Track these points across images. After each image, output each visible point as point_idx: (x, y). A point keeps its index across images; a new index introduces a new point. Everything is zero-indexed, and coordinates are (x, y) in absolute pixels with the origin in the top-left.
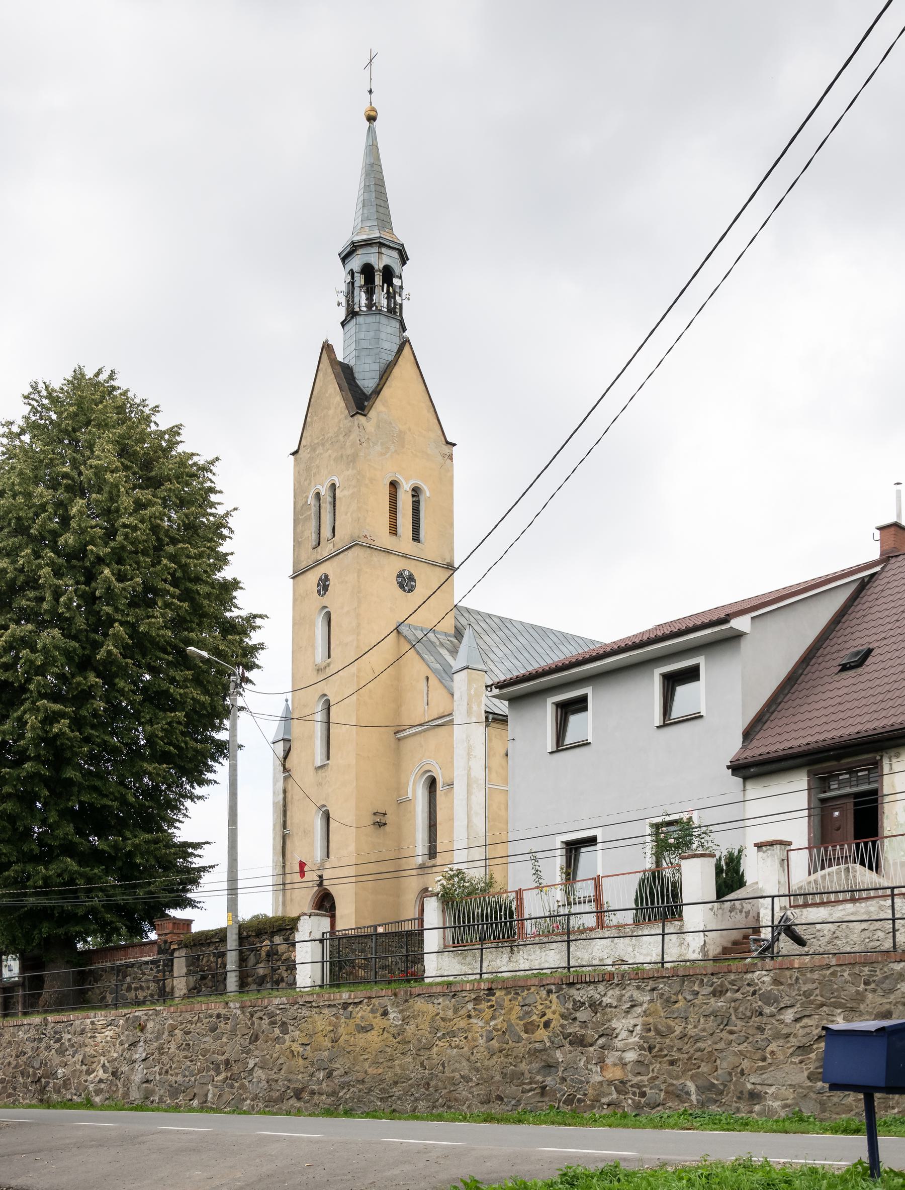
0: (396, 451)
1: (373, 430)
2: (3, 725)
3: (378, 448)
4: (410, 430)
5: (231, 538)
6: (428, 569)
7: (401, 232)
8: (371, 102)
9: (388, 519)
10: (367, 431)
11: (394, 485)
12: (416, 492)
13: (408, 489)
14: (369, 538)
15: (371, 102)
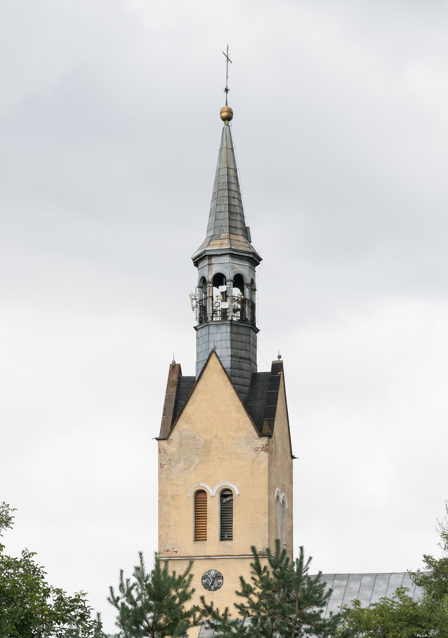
0: (201, 462)
3: (181, 465)
4: (216, 437)
5: (31, 557)
8: (227, 102)
10: (168, 452)
13: (214, 494)
14: (171, 550)
15: (227, 102)
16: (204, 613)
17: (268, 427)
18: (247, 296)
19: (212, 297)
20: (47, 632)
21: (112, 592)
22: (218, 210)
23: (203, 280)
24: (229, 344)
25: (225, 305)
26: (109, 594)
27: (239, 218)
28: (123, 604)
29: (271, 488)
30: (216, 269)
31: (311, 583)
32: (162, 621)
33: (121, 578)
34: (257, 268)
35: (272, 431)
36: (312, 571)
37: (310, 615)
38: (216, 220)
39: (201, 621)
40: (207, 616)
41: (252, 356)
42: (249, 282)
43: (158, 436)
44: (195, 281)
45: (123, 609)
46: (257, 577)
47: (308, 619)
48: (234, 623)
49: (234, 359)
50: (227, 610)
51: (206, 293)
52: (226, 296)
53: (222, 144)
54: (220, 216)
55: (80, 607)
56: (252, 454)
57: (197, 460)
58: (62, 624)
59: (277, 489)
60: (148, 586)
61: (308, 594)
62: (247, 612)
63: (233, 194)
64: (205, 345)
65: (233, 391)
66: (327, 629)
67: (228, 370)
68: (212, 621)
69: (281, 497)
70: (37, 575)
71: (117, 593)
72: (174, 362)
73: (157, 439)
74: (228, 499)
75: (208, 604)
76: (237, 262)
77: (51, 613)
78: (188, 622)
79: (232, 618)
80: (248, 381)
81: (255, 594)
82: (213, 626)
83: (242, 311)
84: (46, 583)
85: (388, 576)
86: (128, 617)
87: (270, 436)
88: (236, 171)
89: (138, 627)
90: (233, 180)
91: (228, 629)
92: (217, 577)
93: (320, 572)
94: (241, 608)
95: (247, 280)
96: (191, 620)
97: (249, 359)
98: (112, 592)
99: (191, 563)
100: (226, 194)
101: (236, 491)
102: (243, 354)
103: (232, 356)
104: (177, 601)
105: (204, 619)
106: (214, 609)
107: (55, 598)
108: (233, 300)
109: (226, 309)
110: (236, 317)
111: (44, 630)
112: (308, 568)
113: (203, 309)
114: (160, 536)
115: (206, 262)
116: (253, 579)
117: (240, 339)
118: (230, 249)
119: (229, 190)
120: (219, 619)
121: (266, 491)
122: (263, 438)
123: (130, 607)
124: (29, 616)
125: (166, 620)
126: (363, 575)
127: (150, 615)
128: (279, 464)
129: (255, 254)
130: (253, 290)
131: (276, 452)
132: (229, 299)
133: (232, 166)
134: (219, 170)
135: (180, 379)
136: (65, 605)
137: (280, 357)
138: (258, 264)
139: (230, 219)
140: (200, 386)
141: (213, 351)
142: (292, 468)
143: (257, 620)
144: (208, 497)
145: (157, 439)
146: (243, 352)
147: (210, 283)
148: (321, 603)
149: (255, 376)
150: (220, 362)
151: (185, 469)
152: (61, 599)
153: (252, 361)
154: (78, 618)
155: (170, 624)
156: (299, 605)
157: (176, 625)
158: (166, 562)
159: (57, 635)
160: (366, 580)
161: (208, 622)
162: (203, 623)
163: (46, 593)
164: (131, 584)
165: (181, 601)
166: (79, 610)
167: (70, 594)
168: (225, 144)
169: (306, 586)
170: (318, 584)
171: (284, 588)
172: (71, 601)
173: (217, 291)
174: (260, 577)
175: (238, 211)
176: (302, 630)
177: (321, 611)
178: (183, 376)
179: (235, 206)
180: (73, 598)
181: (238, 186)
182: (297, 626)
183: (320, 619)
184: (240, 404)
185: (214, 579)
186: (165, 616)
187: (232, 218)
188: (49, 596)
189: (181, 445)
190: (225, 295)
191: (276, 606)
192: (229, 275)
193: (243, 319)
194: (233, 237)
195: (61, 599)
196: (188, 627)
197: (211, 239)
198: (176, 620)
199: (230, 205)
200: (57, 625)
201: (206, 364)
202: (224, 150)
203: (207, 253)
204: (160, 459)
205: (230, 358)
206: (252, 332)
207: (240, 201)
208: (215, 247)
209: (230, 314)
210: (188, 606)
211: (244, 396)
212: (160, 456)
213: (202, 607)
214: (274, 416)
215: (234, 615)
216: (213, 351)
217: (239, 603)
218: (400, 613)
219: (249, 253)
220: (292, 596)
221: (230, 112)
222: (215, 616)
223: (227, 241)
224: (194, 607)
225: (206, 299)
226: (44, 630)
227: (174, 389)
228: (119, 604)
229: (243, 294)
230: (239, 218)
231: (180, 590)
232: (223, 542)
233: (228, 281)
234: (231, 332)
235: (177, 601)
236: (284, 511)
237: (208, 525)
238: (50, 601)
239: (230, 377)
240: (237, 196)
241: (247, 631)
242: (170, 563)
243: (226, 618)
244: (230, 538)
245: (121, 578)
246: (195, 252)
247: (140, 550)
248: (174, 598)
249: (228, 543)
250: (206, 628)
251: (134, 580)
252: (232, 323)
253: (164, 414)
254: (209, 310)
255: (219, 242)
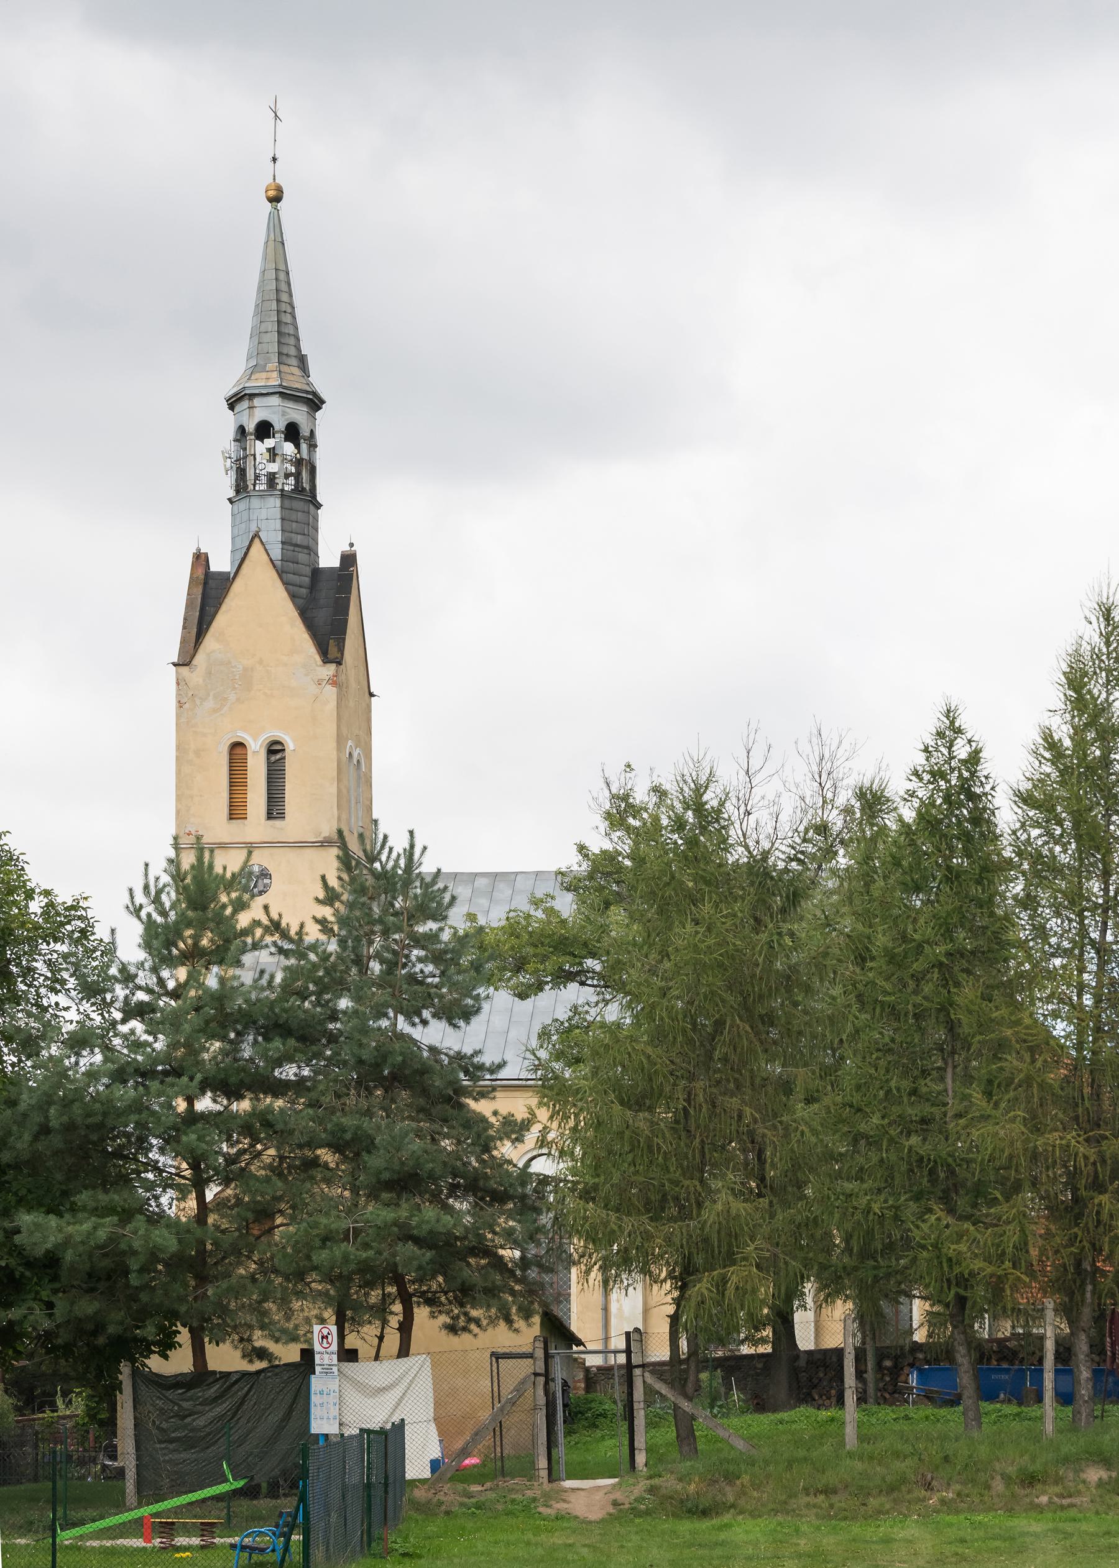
0: (238, 700)
1: (201, 681)
2: (8, 1305)
3: (210, 704)
4: (261, 662)
6: (291, 855)
7: (320, 381)
9: (248, 812)
11: (237, 748)
12: (275, 749)
16: (267, 930)
17: (336, 649)
18: (305, 455)
19: (254, 455)
20: (30, 956)
21: (132, 897)
22: (263, 330)
23: (242, 431)
24: (278, 524)
25: (273, 467)
26: (127, 900)
27: (292, 341)
28: (149, 915)
29: (340, 741)
30: (260, 415)
31: (426, 886)
32: (205, 942)
33: (146, 875)
34: (318, 414)
35: (342, 654)
36: (427, 867)
37: (425, 935)
38: (259, 343)
39: (264, 943)
40: (272, 935)
41: (311, 543)
42: (307, 434)
43: (176, 660)
44: (231, 432)
45: (150, 924)
46: (345, 877)
47: (419, 941)
48: (313, 947)
49: (285, 547)
50: (302, 926)
51: (245, 449)
52: (275, 455)
53: (268, 236)
54: (266, 338)
55: (80, 918)
56: (313, 689)
57: (232, 697)
58: (52, 944)
59: (350, 743)
60: (185, 888)
61: (423, 902)
62: (332, 930)
63: (284, 307)
64: (243, 525)
65: (285, 594)
66: (449, 956)
67: (278, 563)
68: (279, 943)
69: (355, 755)
70: (15, 865)
71: (140, 898)
72: (199, 550)
73: (175, 665)
74: (278, 756)
75: (275, 917)
76: (291, 404)
77: (37, 926)
78: (245, 943)
79: (309, 939)
80: (306, 580)
81: (342, 902)
82: (281, 951)
83: (297, 476)
84: (29, 880)
85: (513, 876)
86: (157, 936)
87: (339, 663)
88: (288, 273)
89: (170, 952)
90: (284, 287)
91: (302, 956)
92: (262, 875)
93: (439, 870)
94: (322, 922)
95: (305, 431)
96: (249, 940)
97: (308, 548)
98: (132, 897)
99: (250, 853)
100: (274, 306)
101: (290, 745)
102: (299, 539)
103: (283, 543)
104: (228, 911)
105: (269, 939)
106: (283, 924)
107: (43, 904)
108: (284, 460)
109: (275, 473)
110: (289, 485)
111: (25, 953)
112: (420, 864)
113: (241, 473)
114: (178, 812)
115: (245, 404)
116: (340, 878)
117: (294, 517)
118: (280, 386)
119: (278, 301)
120: (291, 940)
121: (335, 744)
122: (328, 665)
123: (159, 919)
124: (7, 932)
125: (212, 940)
126: (476, 874)
127: (188, 932)
128: (352, 704)
129: (315, 394)
130: (313, 446)
131: (347, 687)
132: (278, 459)
133: (282, 267)
134: (263, 272)
135: (208, 576)
136: (58, 914)
137: (352, 545)
138: (319, 408)
139: (279, 342)
140: (237, 587)
141: (256, 535)
142: (370, 711)
143: (346, 942)
144: (249, 753)
145: (175, 665)
146: (299, 537)
147: (251, 434)
148: (439, 915)
149: (317, 572)
150: (266, 550)
151: (215, 711)
152: (51, 905)
153: (311, 550)
154: (77, 935)
155: (218, 946)
156: (408, 920)
157: (229, 949)
158: (212, 851)
159: (45, 961)
160: (481, 882)
161: (275, 944)
162: (267, 946)
163: (30, 895)
164: (161, 885)
165: (235, 911)
166: (79, 923)
167: (64, 897)
168: (272, 235)
169: (419, 891)
170: (436, 888)
171: (386, 893)
172: (66, 909)
173: (261, 448)
174: (349, 876)
175: (292, 332)
176: (413, 958)
177: (441, 929)
178: (212, 569)
179: (286, 324)
180: (69, 904)
181: (291, 295)
182: (406, 952)
183: (440, 942)
184: (295, 614)
185: (258, 877)
186: (210, 934)
187: (283, 341)
188: (33, 899)
189: (209, 673)
190: (273, 453)
191: (375, 920)
192: (279, 424)
193: (298, 489)
194: (284, 368)
195: (51, 905)
196: (244, 952)
197: (254, 370)
198: (228, 941)
199: (279, 322)
200: (44, 946)
201: (246, 554)
202: (271, 244)
203: (247, 392)
204: (178, 695)
205: (280, 546)
206: (312, 507)
207: (294, 318)
208: (258, 382)
209: (280, 481)
210: (244, 920)
211: (300, 601)
212: (178, 690)
213: (265, 921)
214: (345, 633)
215: (313, 933)
216: (256, 535)
217: (319, 916)
218: (542, 934)
219: (307, 392)
220: (397, 905)
221: (280, 190)
222: (285, 935)
223: (275, 374)
224: (254, 921)
225: (245, 457)
226: (25, 953)
227: (199, 591)
228: (143, 914)
229: (299, 452)
230: (292, 341)
231: (234, 895)
232: (271, 822)
233: (278, 432)
234: (282, 507)
235: (228, 911)
236: (359, 778)
237: (248, 796)
238: (35, 906)
239: (281, 573)
240: (289, 310)
241: (332, 959)
242: (217, 852)
243: (301, 940)
244: (281, 816)
245: (146, 875)
246: (230, 388)
247: (388, 833)
248: (224, 907)
249: (277, 823)
250: (271, 954)
251: (165, 879)
252: (283, 495)
253: (184, 628)
254: (250, 475)
255: (264, 375)
